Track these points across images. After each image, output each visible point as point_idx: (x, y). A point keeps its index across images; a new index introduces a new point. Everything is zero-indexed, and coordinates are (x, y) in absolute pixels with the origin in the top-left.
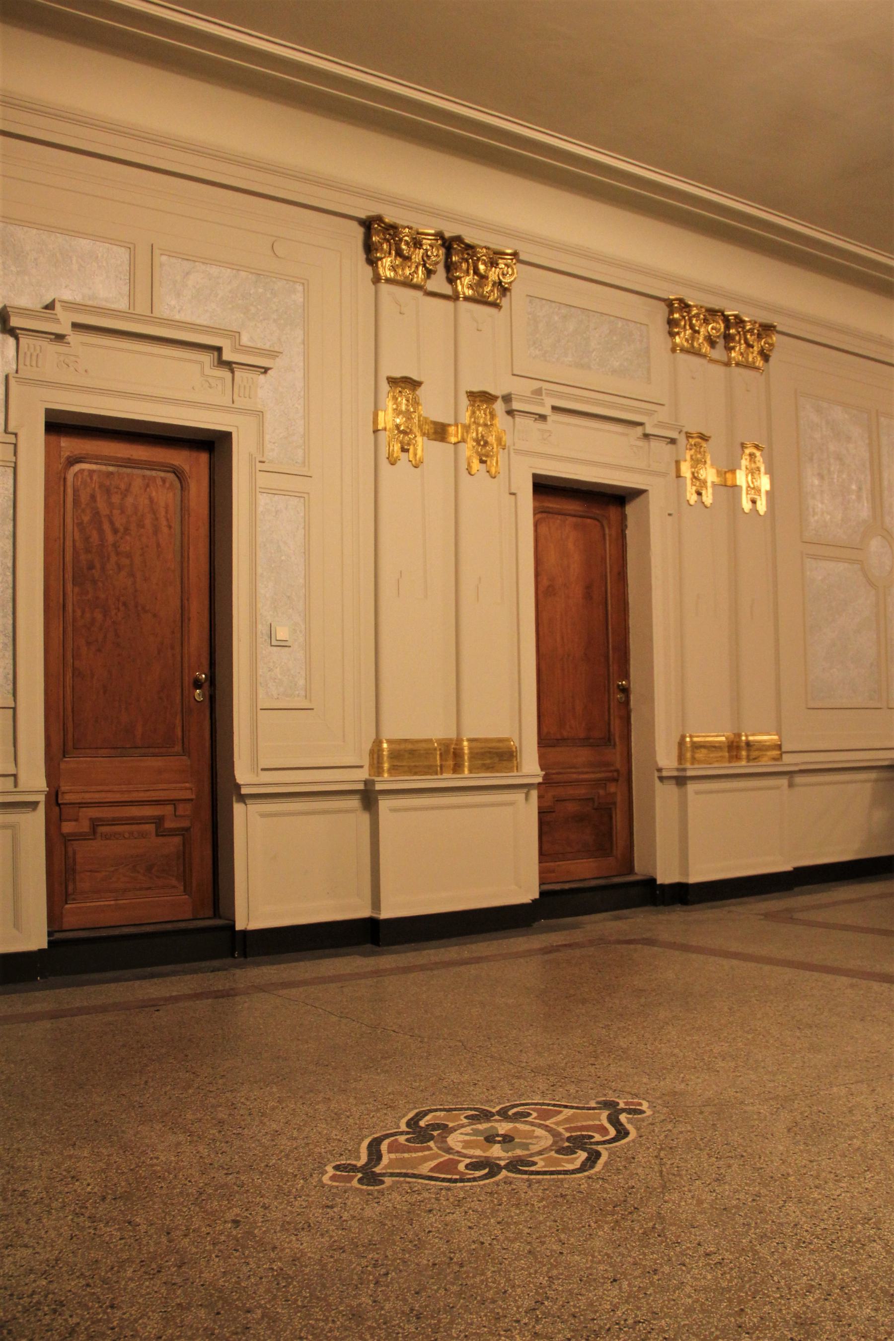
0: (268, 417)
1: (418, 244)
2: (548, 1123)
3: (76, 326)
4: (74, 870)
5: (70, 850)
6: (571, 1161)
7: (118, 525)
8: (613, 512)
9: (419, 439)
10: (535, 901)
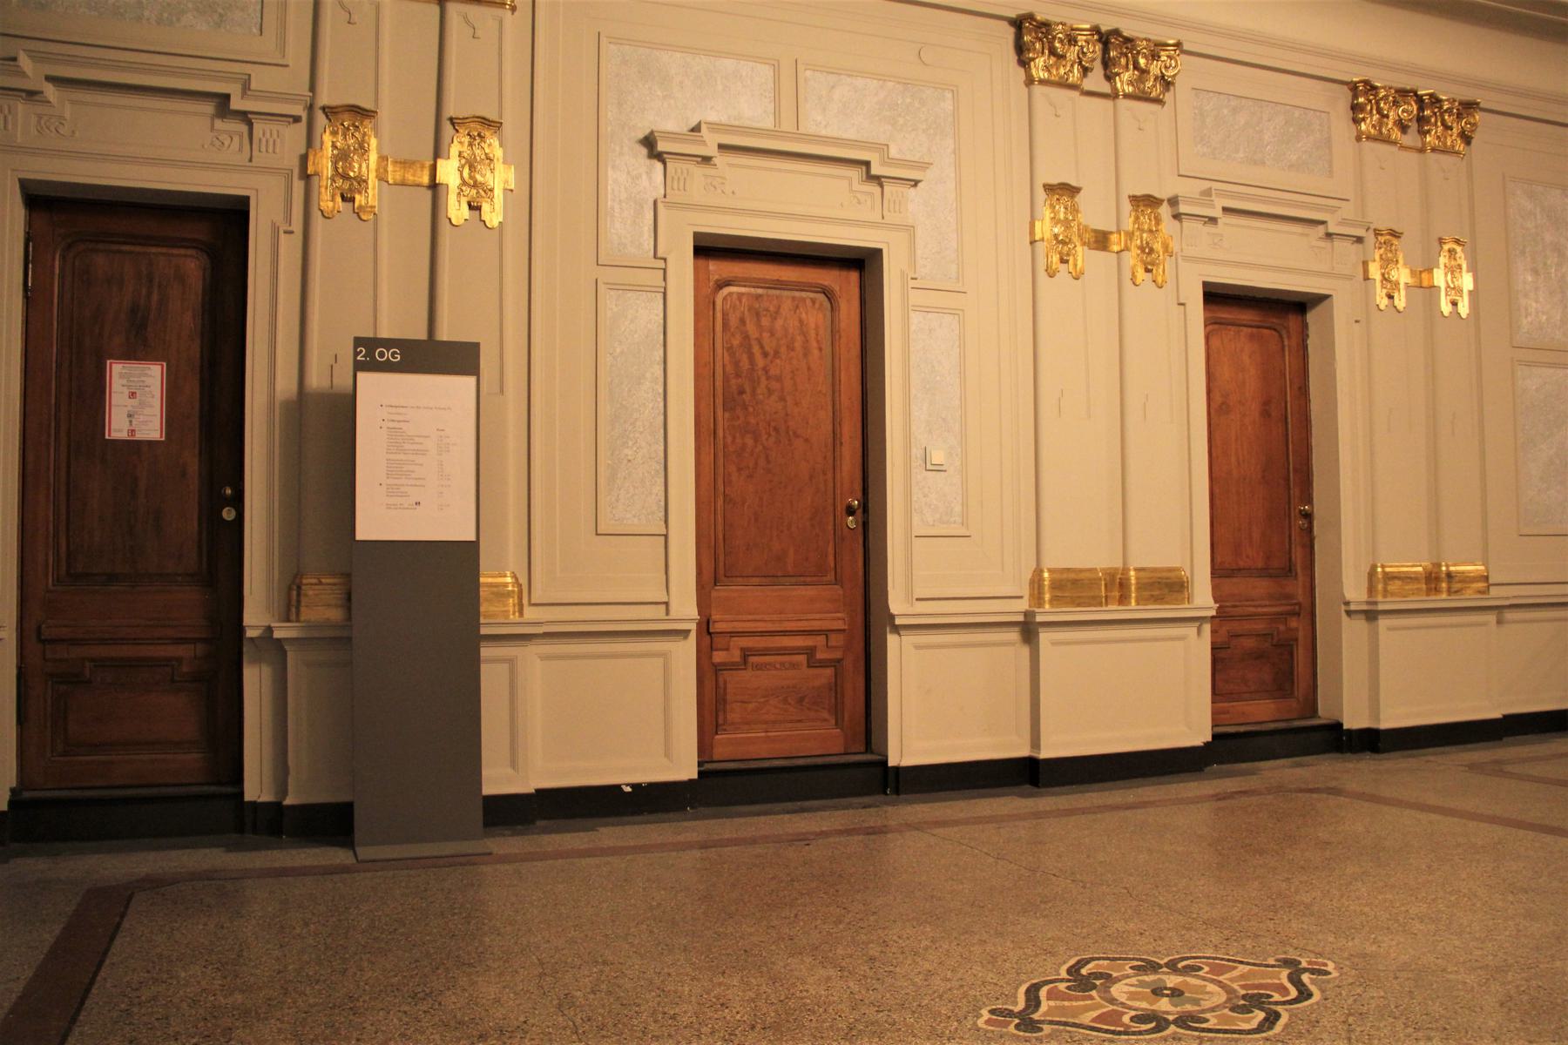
1: (1072, 41)
3: (721, 147)
4: (725, 701)
5: (721, 680)
6: (1248, 1021)
7: (767, 348)
8: (1292, 321)
9: (1079, 249)
10: (1207, 744)
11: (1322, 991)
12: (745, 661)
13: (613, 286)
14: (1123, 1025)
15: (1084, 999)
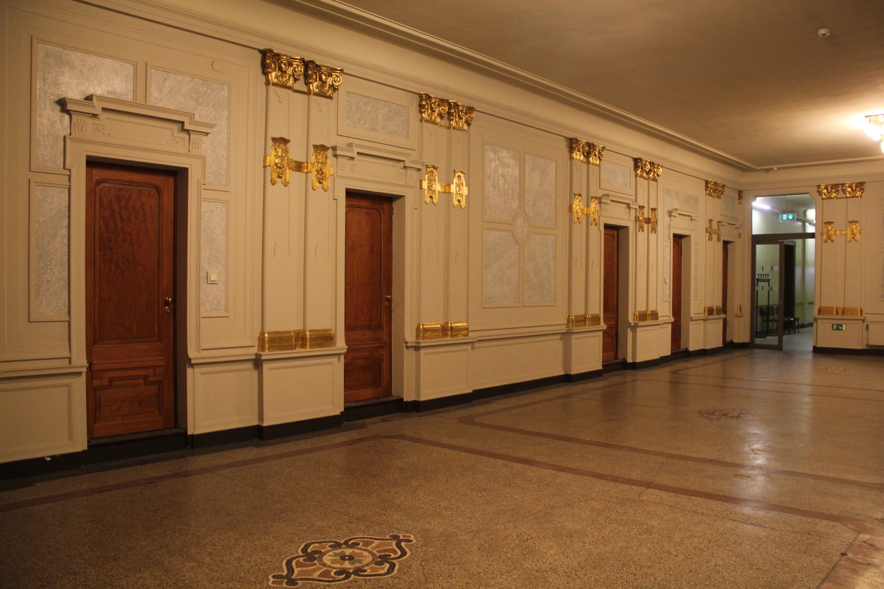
0: (208, 159)
2: (368, 548)
6: (383, 569)
8: (386, 206)
9: (288, 171)
11: (411, 550)
12: (111, 385)
13: (39, 184)
14: (332, 577)
15: (312, 565)
